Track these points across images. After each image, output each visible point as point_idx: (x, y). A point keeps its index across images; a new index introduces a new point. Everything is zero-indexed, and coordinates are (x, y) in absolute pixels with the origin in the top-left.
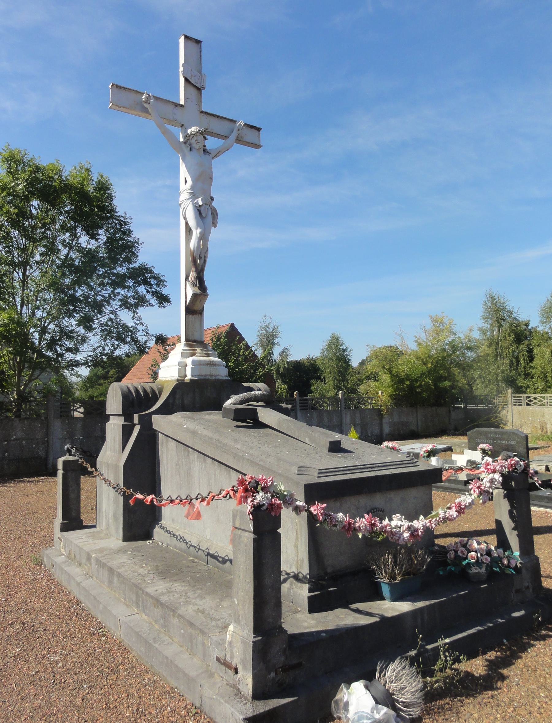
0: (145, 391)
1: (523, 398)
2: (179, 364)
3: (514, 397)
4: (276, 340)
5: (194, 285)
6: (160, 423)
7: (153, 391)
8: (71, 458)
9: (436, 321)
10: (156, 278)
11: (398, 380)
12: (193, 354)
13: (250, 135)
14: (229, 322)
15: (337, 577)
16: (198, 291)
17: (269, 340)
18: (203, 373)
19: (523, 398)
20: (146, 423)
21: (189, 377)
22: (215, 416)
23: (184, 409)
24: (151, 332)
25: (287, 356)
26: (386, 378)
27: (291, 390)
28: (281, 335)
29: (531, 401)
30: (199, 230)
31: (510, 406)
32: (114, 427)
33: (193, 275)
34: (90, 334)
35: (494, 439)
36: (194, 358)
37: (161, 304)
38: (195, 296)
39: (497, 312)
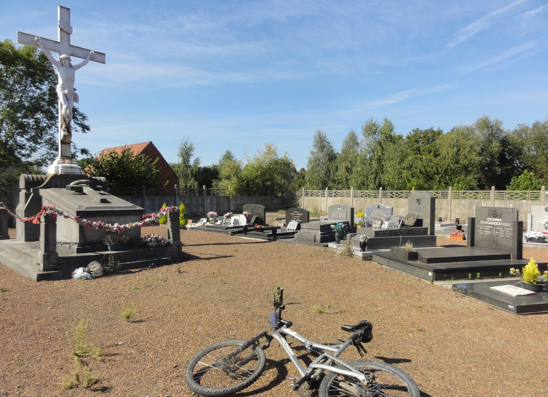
2: (56, 167)
4: (192, 153)
5: (64, 131)
6: (43, 192)
7: (42, 178)
8: (3, 208)
9: (269, 148)
10: (81, 115)
11: (241, 180)
12: (64, 163)
13: (99, 57)
14: (149, 141)
15: (91, 244)
16: (66, 133)
17: (186, 153)
18: (67, 171)
20: (36, 193)
21: (60, 173)
22: (64, 190)
23: (56, 186)
24: (77, 147)
25: (198, 163)
26: (234, 179)
27: (200, 186)
28: (195, 150)
30: (65, 106)
32: (22, 193)
33: (64, 126)
34: (38, 146)
35: (253, 209)
36: (64, 165)
37: (84, 131)
38: (65, 136)
39: (322, 143)
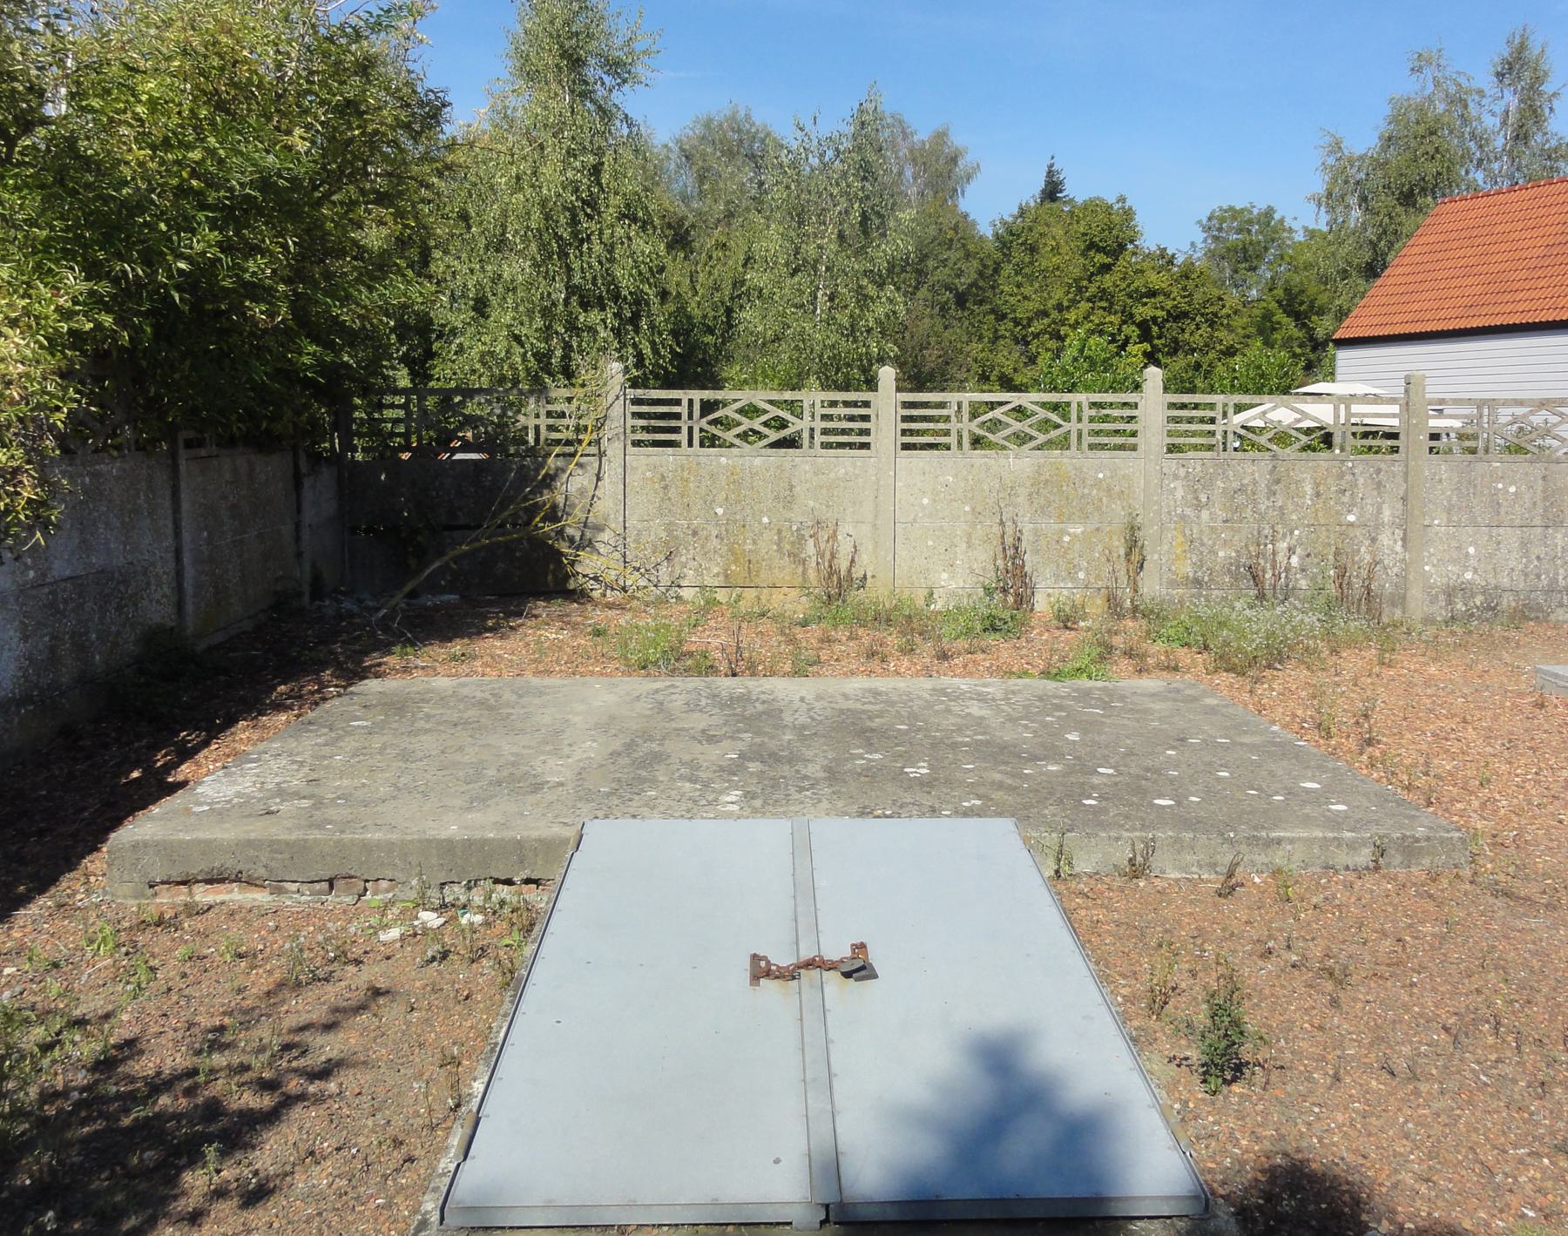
0: (1282, 221)
1: (683, 409)
3: (637, 401)
19: (683, 409)
29: (995, 425)
31: (614, 450)
